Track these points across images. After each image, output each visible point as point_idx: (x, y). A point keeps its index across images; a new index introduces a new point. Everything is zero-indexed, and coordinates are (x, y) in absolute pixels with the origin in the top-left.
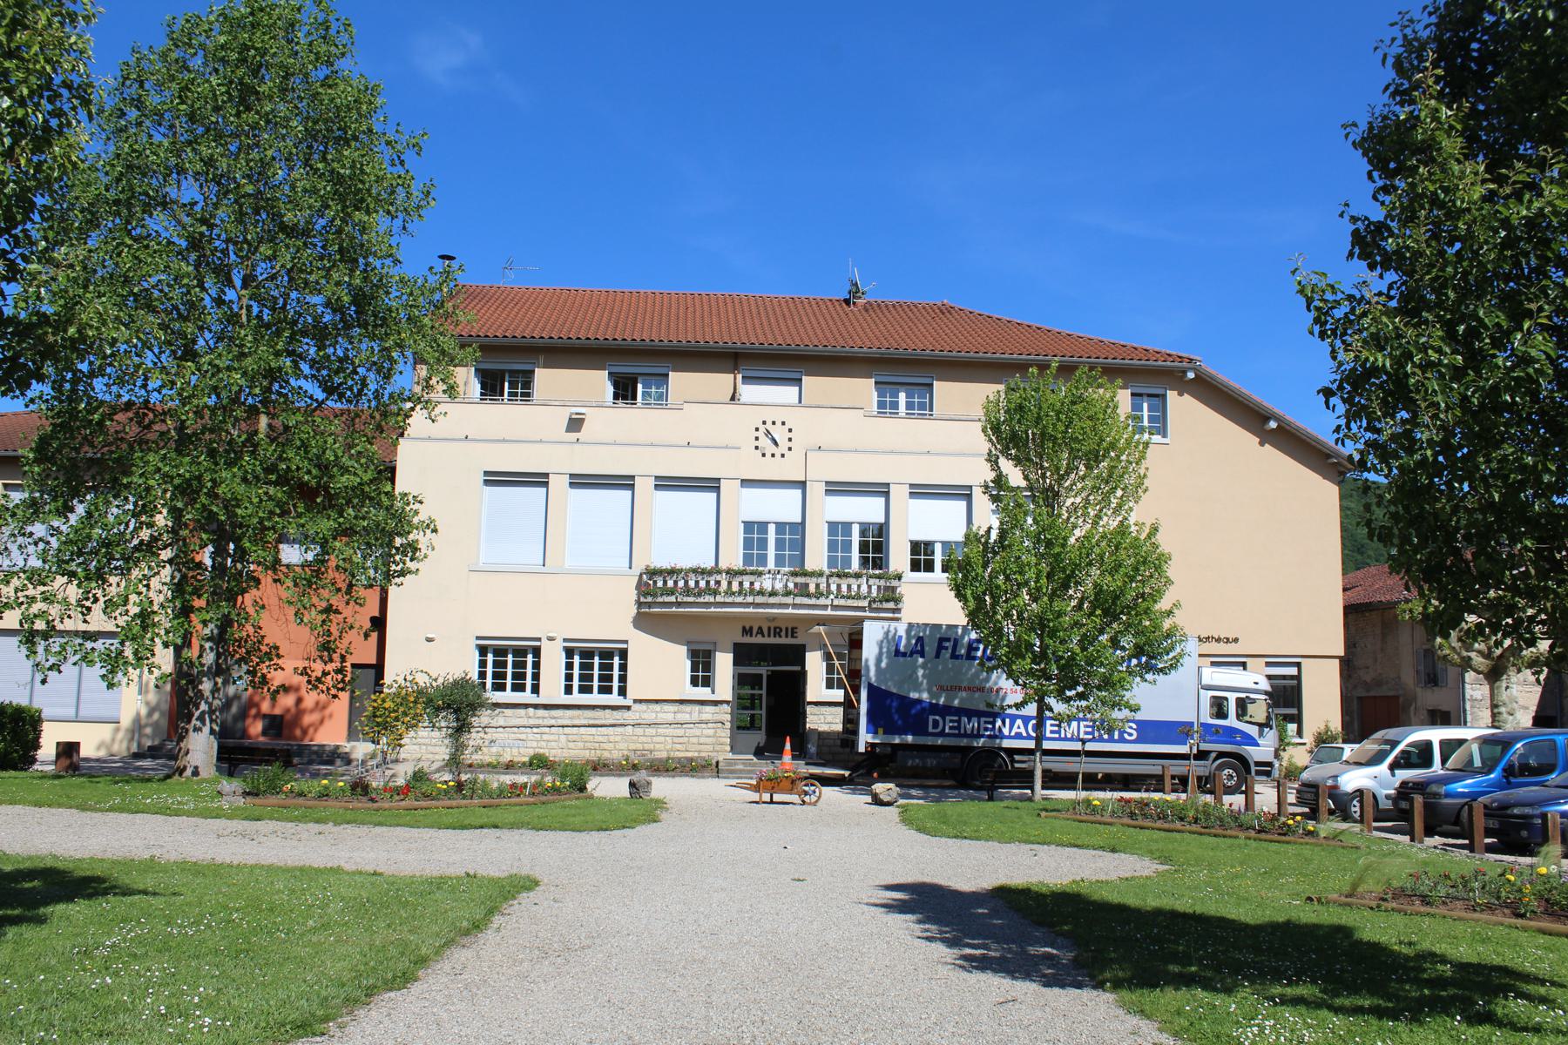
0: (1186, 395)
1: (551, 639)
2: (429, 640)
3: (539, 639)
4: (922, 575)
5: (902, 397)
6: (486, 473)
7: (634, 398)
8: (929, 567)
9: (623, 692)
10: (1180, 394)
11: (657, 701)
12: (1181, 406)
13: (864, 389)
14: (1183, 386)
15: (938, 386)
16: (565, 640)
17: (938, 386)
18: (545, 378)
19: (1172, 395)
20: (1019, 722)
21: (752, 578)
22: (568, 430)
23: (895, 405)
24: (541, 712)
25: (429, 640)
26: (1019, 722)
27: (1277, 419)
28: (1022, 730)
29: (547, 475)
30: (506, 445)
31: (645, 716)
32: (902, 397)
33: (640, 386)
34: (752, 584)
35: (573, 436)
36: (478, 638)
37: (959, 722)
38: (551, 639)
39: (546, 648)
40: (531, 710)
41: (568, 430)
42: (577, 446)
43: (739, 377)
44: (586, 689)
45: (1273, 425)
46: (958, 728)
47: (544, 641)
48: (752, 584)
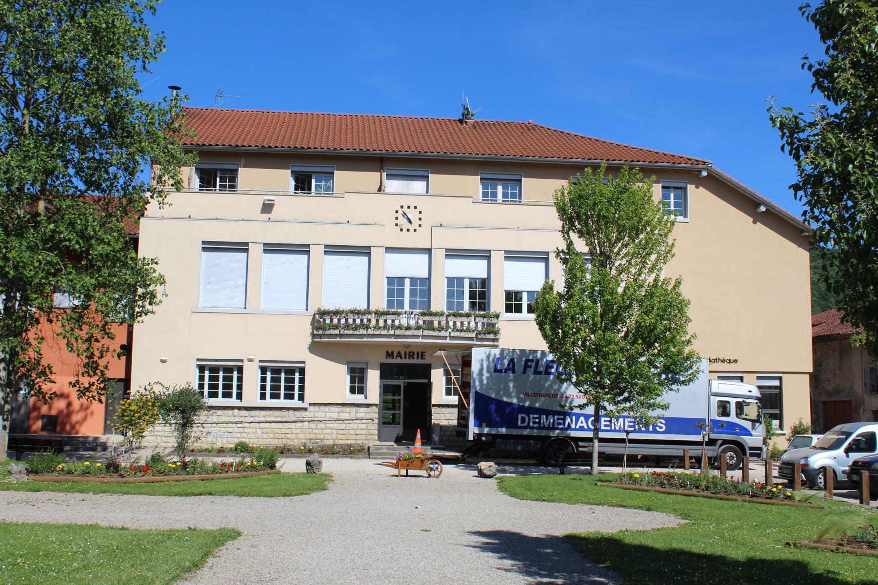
0: (701, 189)
1: (250, 360)
2: (163, 361)
3: (242, 361)
5: (500, 189)
6: (204, 243)
8: (519, 309)
9: (239, 396)
10: (697, 187)
13: (472, 183)
14: (699, 181)
18: (246, 175)
19: (691, 188)
20: (582, 418)
21: (393, 317)
23: (494, 195)
24: (243, 413)
26: (582, 418)
27: (766, 205)
29: (247, 244)
31: (317, 415)
32: (500, 189)
36: (198, 360)
38: (250, 360)
39: (247, 367)
40: (236, 411)
42: (268, 223)
43: (384, 174)
44: (275, 396)
45: (763, 208)
47: (245, 362)
48: (393, 321)
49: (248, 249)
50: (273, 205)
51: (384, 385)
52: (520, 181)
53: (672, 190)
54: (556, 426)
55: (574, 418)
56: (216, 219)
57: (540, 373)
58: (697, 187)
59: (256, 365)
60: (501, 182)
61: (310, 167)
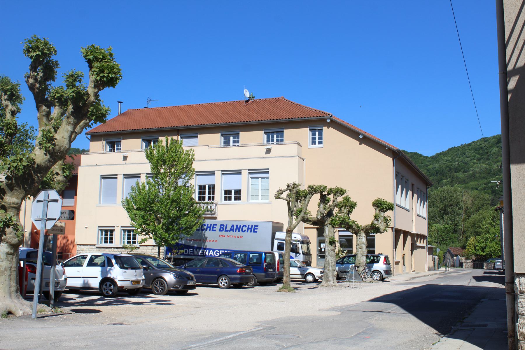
1: (117, 227)
2: (86, 228)
4: (228, 202)
5: (232, 138)
6: (101, 176)
7: (114, 150)
8: (230, 199)
9: (111, 242)
10: (328, 128)
11: (91, 245)
13: (217, 138)
14: (328, 125)
15: (286, 131)
17: (286, 131)
19: (325, 129)
20: (211, 251)
21: (211, 205)
22: (266, 154)
23: (229, 142)
24: (115, 250)
26: (211, 251)
27: (362, 134)
29: (214, 171)
30: (259, 159)
32: (232, 138)
34: (211, 207)
35: (125, 162)
37: (193, 251)
38: (117, 227)
39: (116, 228)
41: (266, 154)
42: (125, 165)
43: (179, 137)
44: (106, 242)
45: (361, 137)
46: (193, 253)
48: (211, 207)
50: (270, 150)
52: (120, 141)
56: (106, 165)
57: (228, 231)
58: (328, 128)
59: (119, 228)
61: (274, 128)
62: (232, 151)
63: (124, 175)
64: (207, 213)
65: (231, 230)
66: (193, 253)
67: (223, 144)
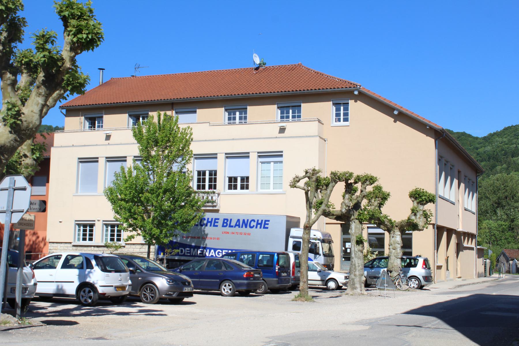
0: (359, 102)
1: (98, 221)
2: (60, 222)
3: (94, 221)
4: (233, 191)
5: (238, 113)
6: (79, 159)
7: (95, 127)
8: (235, 188)
9: (91, 239)
10: (356, 101)
12: (356, 107)
13: (219, 113)
14: (356, 98)
15: (303, 105)
16: (103, 221)
17: (303, 105)
18: (107, 118)
19: (351, 102)
20: (212, 251)
21: (212, 195)
23: (234, 119)
24: (96, 249)
25: (60, 222)
26: (212, 251)
27: (397, 110)
28: (214, 254)
31: (130, 250)
32: (238, 113)
33: (96, 122)
34: (212, 197)
35: (108, 142)
36: (76, 221)
37: (190, 250)
38: (98, 221)
39: (96, 223)
40: (93, 248)
43: (174, 112)
44: (84, 239)
45: (396, 112)
46: (190, 253)
47: (96, 221)
48: (212, 197)
49: (282, 155)
51: (344, 239)
53: (342, 105)
54: (186, 254)
55: (208, 250)
57: (232, 226)
58: (356, 101)
60: (291, 108)
61: (290, 101)
62: (238, 129)
63: (107, 158)
64: (208, 204)
65: (236, 225)
66: (190, 253)
67: (227, 121)
